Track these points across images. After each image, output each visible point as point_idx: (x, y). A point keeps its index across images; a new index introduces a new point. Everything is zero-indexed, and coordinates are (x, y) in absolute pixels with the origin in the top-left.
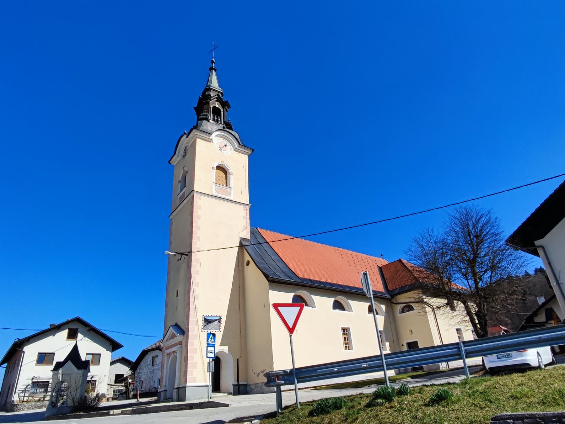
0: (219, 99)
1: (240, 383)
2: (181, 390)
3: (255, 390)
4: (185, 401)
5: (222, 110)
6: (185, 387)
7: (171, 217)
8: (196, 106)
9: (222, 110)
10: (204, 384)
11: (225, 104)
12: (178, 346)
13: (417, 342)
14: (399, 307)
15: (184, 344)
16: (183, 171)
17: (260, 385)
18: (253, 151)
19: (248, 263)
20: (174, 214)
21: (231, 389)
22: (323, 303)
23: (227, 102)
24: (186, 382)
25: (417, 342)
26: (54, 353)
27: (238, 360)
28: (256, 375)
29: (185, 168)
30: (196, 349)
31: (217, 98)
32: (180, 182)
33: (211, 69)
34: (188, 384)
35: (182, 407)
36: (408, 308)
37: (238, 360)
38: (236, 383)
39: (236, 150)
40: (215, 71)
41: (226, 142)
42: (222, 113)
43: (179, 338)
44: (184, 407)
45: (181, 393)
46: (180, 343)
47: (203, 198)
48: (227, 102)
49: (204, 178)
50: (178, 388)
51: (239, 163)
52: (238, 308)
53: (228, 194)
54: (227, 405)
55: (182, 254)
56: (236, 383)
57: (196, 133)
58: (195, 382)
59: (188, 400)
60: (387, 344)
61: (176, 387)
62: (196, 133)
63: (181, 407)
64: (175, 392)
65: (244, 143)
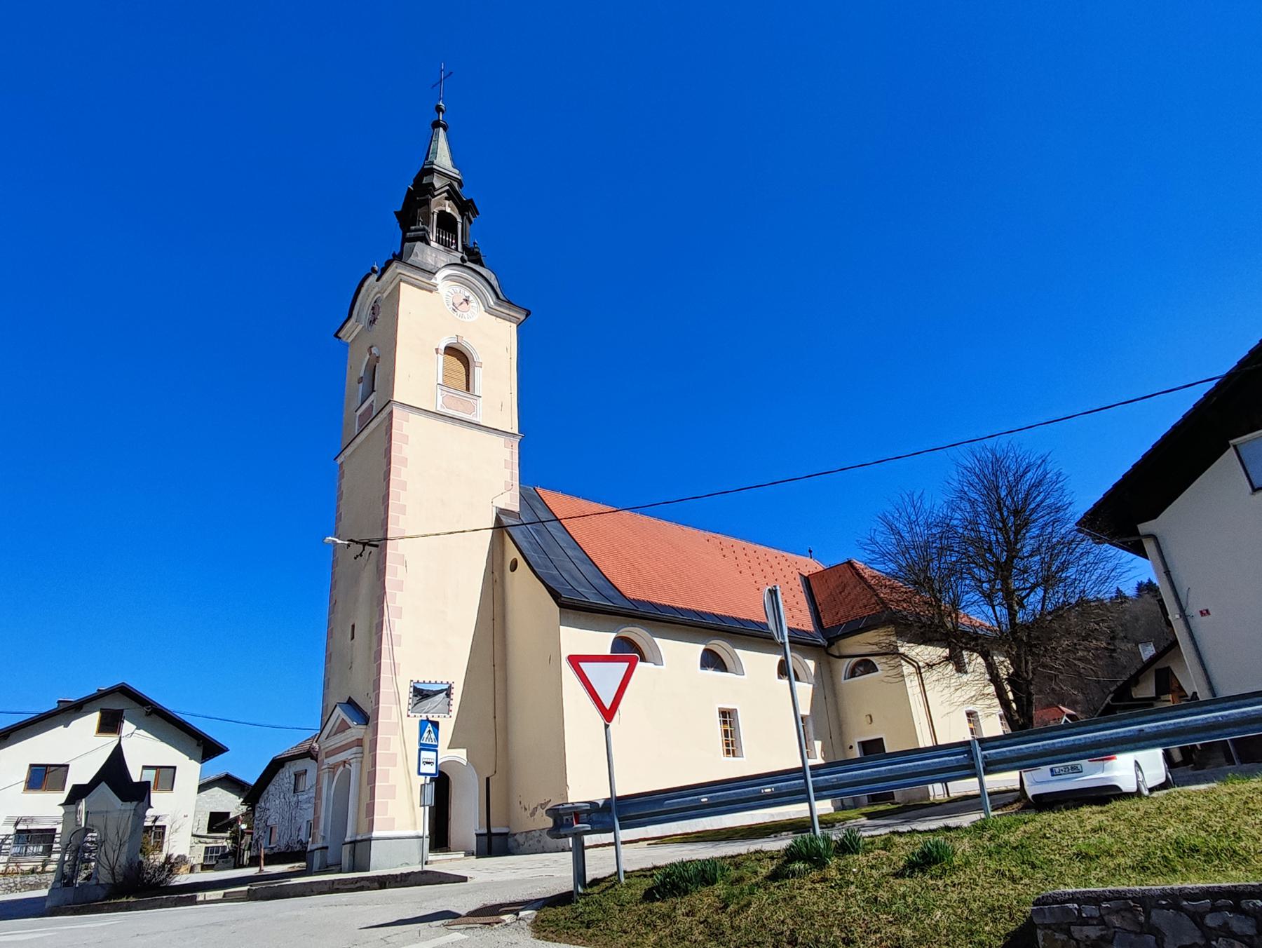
0: (452, 195)
1: (493, 830)
6: (370, 840)
7: (339, 461)
8: (399, 209)
10: (413, 833)
11: (466, 207)
12: (354, 749)
14: (846, 664)
19: (514, 566)
21: (473, 846)
22: (679, 655)
23: (471, 200)
24: (371, 829)
26: (67, 766)
27: (488, 779)
28: (528, 813)
29: (374, 350)
33: (436, 125)
34: (376, 833)
35: (363, 883)
36: (865, 666)
37: (488, 779)
39: (489, 310)
40: (445, 129)
42: (460, 226)
43: (356, 731)
44: (367, 884)
46: (359, 743)
49: (415, 374)
50: (354, 842)
51: (496, 341)
52: (490, 663)
53: (473, 410)
54: (464, 879)
55: (364, 544)
58: (392, 829)
60: (818, 745)
64: (346, 850)
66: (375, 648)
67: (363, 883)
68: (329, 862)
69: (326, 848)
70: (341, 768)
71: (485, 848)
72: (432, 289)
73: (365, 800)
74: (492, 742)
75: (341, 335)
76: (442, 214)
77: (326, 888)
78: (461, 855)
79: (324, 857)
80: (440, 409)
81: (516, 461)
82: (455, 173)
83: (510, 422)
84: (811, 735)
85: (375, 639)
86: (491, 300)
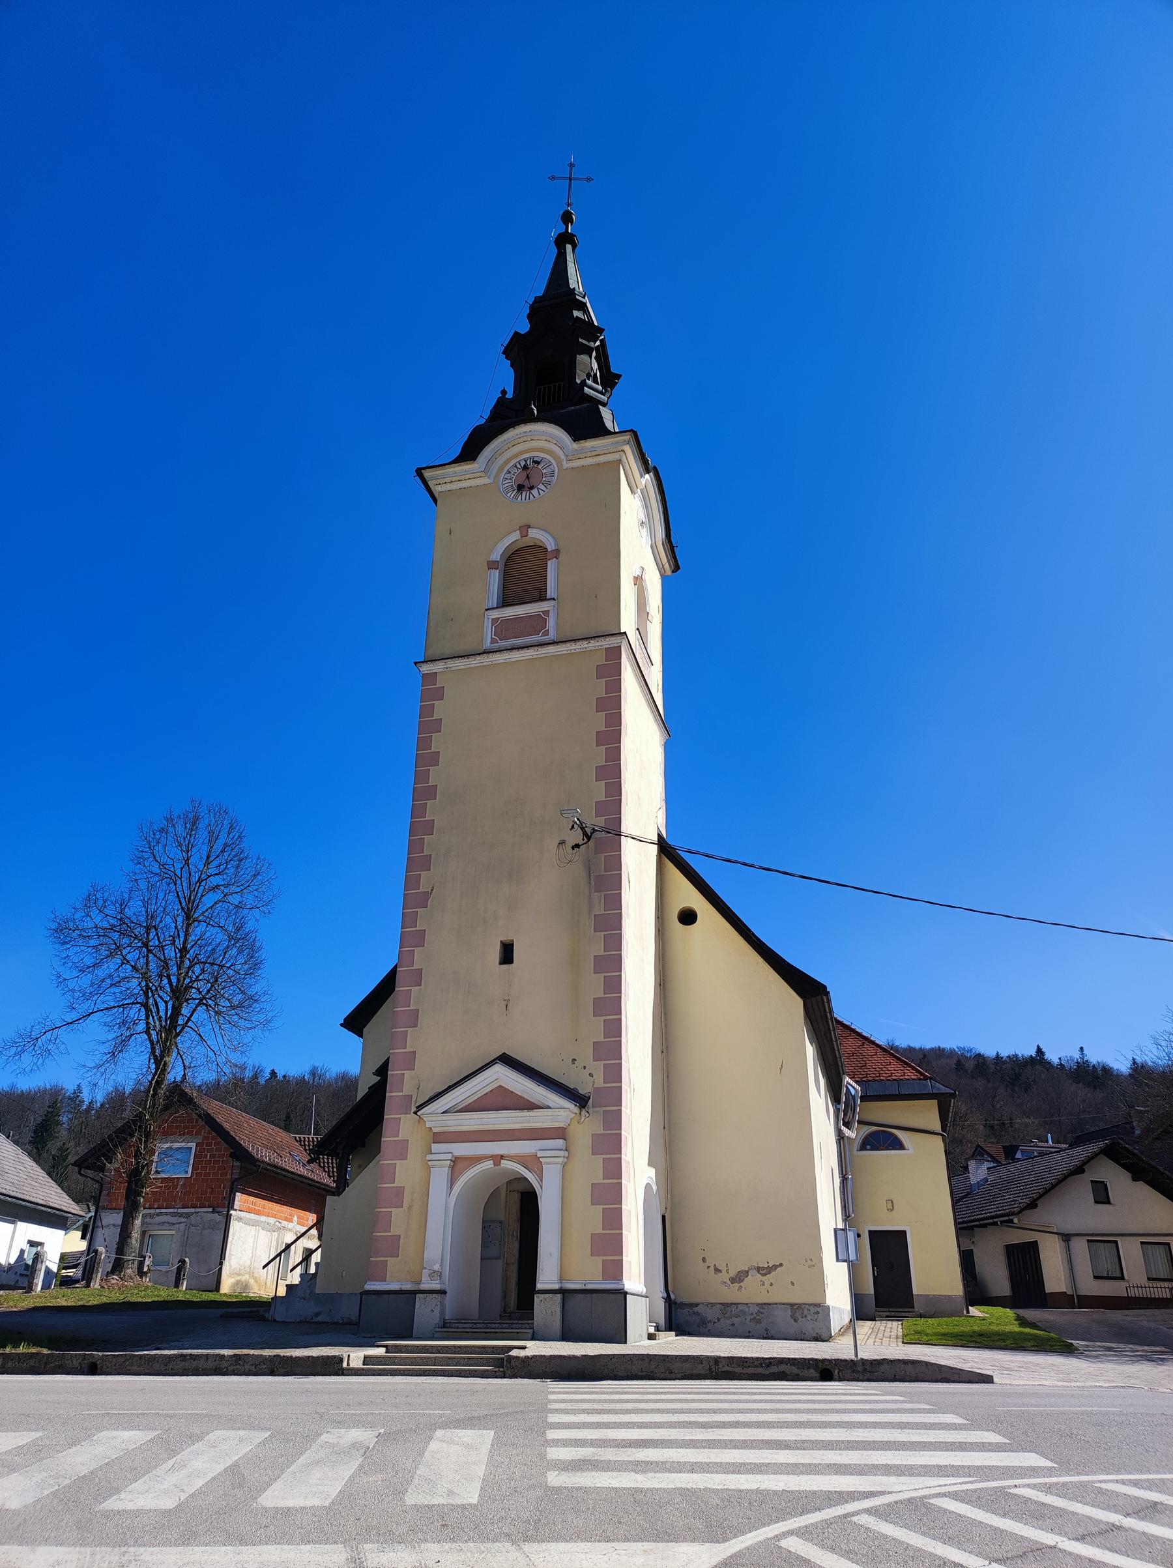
2: (576, 1302)
16: (516, 536)
20: (459, 664)
25: (903, 1233)
26: (1108, 1202)
28: (725, 1277)
32: (492, 565)
35: (782, 1368)
37: (664, 1217)
39: (653, 547)
43: (561, 1111)
44: (795, 1370)
46: (559, 1133)
54: (988, 1379)
62: (627, 448)
63: (774, 1369)
69: (443, 1292)
70: (489, 1164)
85: (594, 986)
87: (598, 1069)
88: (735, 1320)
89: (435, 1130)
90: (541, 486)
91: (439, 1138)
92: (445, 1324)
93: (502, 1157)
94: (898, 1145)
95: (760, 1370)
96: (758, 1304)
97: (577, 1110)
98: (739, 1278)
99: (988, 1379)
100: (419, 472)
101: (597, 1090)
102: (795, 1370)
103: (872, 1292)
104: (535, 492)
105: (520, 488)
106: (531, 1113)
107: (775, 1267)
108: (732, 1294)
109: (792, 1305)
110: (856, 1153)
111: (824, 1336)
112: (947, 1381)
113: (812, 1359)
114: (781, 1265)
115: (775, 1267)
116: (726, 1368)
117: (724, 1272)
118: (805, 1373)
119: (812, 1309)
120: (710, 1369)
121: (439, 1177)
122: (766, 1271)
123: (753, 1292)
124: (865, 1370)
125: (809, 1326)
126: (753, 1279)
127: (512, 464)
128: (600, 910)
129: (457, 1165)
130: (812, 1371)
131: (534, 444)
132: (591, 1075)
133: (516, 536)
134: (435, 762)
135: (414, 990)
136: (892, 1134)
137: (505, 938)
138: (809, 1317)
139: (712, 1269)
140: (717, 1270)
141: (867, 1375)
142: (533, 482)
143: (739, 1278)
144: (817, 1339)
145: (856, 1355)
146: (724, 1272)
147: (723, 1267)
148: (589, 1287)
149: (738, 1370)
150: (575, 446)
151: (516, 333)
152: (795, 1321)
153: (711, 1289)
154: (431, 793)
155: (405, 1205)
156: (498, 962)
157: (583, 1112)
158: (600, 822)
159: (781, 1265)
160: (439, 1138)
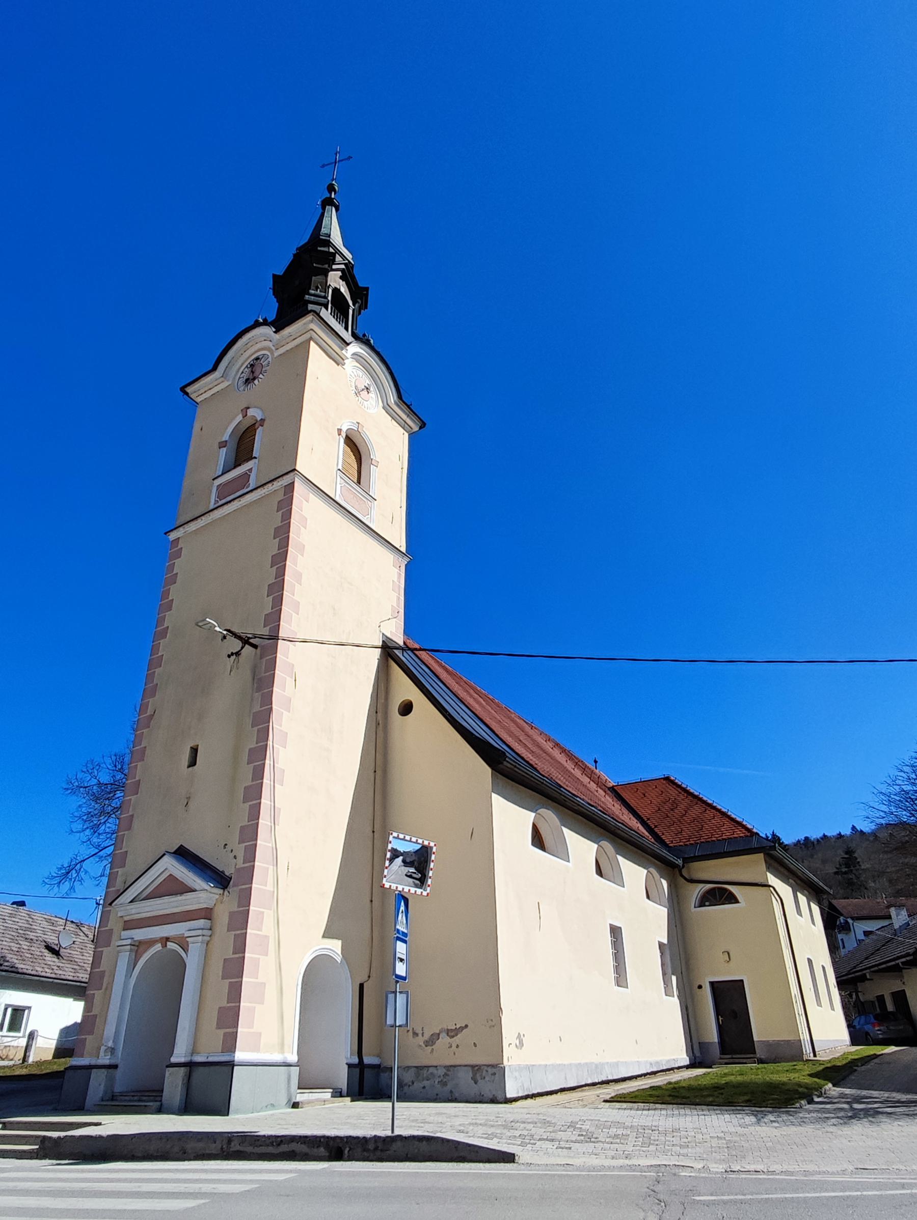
0: (348, 275)
1: (367, 1060)
2: (199, 1072)
3: (418, 1085)
4: (222, 1109)
5: (351, 303)
6: (231, 1065)
7: (173, 536)
8: (280, 272)
9: (351, 303)
10: (277, 1057)
11: (360, 294)
12: (201, 923)
13: (742, 981)
14: (697, 890)
15: (222, 917)
16: (240, 418)
17: (441, 1072)
18: (423, 425)
19: (406, 709)
20: (193, 527)
21: (343, 1082)
23: (367, 289)
24: (230, 1043)
25: (742, 981)
26: (324, 937)
27: (361, 986)
28: (420, 1040)
29: (250, 412)
30: (267, 937)
31: (342, 270)
32: (223, 445)
33: (328, 202)
34: (240, 1055)
35: (294, 1146)
36: (720, 895)
37: (361, 986)
38: (356, 1060)
39: (387, 408)
40: (337, 210)
41: (366, 381)
43: (204, 894)
44: (303, 1148)
45: (208, 1086)
46: (207, 914)
47: (315, 501)
48: (367, 289)
49: (317, 454)
50: (190, 1065)
51: (390, 444)
52: (370, 829)
54: (508, 1158)
55: (246, 641)
56: (356, 1060)
57: (312, 326)
58: (257, 1049)
59: (237, 1112)
60: (674, 978)
61: (180, 1055)
62: (312, 326)
63: (284, 1148)
65: (408, 398)
66: (247, 780)
67: (294, 1146)
68: (118, 1089)
69: (115, 1067)
70: (158, 947)
71: (356, 1088)
72: (339, 361)
73: (217, 998)
74: (368, 932)
75: (189, 390)
76: (336, 291)
77: (214, 1148)
78: (327, 1095)
79: (111, 1081)
80: (337, 499)
81: (403, 586)
82: (349, 256)
83: (400, 540)
84: (669, 970)
85: (247, 771)
86: (392, 397)
87: (240, 851)
88: (426, 1083)
89: (126, 919)
90: (261, 376)
91: (129, 925)
92: (113, 1098)
93: (167, 939)
94: (732, 899)
95: (271, 1150)
96: (445, 1067)
97: (221, 891)
98: (432, 1041)
99: (508, 1158)
100: (183, 389)
101: (238, 870)
102: (303, 1148)
103: (716, 1040)
104: (256, 382)
105: (247, 381)
106: (183, 897)
107: (462, 1029)
108: (425, 1057)
109: (473, 1067)
110: (693, 910)
111: (500, 1097)
112: (489, 1161)
113: (324, 1137)
114: (466, 1026)
115: (462, 1029)
116: (238, 1148)
117: (420, 1035)
118: (315, 1151)
119: (489, 1069)
120: (222, 1148)
121: (124, 959)
122: (452, 1033)
123: (442, 1055)
124: (376, 1148)
125: (486, 1088)
126: (444, 1040)
127: (244, 366)
128: (257, 708)
129: (139, 947)
130: (322, 1149)
131: (259, 346)
132: (235, 857)
133: (240, 418)
134: (170, 608)
135: (133, 798)
136: (726, 890)
137: (192, 744)
138: (487, 1079)
139: (411, 1033)
140: (415, 1034)
141: (378, 1153)
142: (256, 374)
143: (432, 1041)
144: (493, 1101)
145: (393, 1132)
146: (420, 1035)
147: (420, 1032)
148: (211, 1059)
149: (249, 1149)
150: (277, 336)
151: (274, 276)
152: (476, 1083)
153: (406, 1053)
154: (164, 634)
155: (104, 987)
156: (187, 764)
157: (226, 892)
158: (265, 631)
159: (466, 1026)
160: (129, 925)
